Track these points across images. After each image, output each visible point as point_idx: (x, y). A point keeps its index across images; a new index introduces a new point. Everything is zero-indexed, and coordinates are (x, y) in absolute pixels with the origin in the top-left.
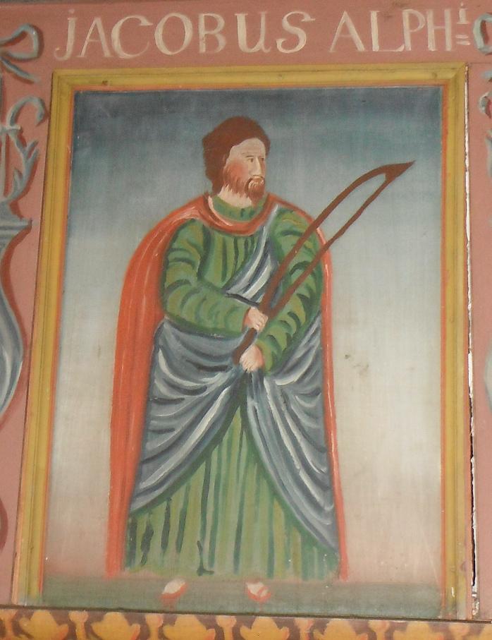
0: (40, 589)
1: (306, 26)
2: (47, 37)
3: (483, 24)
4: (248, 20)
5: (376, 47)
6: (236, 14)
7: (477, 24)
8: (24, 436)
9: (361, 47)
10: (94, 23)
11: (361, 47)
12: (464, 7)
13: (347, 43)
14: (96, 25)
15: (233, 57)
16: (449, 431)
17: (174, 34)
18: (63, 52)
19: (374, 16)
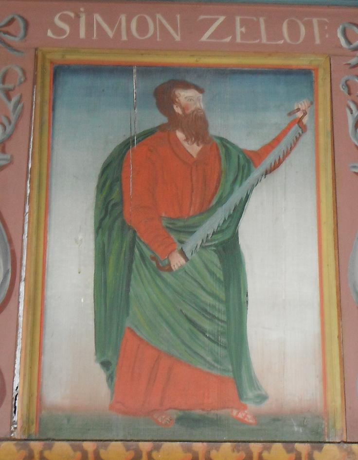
10: (157, 18)
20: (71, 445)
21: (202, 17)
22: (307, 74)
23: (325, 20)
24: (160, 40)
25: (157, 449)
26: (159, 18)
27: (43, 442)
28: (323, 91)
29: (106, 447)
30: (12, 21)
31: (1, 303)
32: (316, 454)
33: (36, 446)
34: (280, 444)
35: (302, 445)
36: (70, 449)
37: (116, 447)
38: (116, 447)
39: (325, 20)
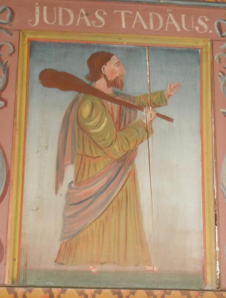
0: (107, 182)
1: (206, 22)
2: (16, 16)
3: (219, 25)
4: (48, 11)
5: (152, 27)
6: (59, 8)
7: (216, 24)
8: (149, 149)
9: (145, 27)
10: (81, 11)
11: (145, 27)
12: (38, 6)
13: (172, 26)
14: (170, 17)
15: (172, 31)
16: (22, 150)
17: (66, 17)
18: (34, 22)
19: (183, 16)
20: (112, 291)
21: (115, 11)
22: (193, 51)
23: (130, 12)
24: (135, 28)
25: (63, 292)
26: (137, 16)
27: (94, 289)
28: (206, 66)
29: (100, 293)
30: (4, 10)
31: (1, 196)
32: (97, 295)
33: (20, 291)
34: (5, 288)
35: (159, 291)
36: (76, 295)
37: (141, 293)
38: (141, 293)
39: (130, 12)
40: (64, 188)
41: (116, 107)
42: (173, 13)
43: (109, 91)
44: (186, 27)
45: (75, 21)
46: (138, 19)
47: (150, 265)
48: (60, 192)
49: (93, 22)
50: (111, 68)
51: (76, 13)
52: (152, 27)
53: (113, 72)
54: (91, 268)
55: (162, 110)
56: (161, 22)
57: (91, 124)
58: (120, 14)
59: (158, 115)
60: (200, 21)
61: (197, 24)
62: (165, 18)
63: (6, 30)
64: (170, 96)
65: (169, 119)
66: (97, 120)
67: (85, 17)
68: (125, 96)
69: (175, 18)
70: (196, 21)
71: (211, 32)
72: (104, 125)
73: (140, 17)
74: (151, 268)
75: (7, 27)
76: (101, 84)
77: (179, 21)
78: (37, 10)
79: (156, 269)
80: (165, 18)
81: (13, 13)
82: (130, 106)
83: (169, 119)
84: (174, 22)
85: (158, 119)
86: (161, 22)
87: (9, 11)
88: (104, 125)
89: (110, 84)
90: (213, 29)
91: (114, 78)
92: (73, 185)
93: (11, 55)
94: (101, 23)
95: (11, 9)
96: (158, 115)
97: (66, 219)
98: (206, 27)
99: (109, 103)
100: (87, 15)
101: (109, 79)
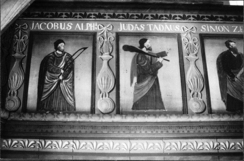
17: (131, 27)
18: (32, 28)
19: (82, 24)
21: (233, 27)
40: (133, 85)
41: (150, 57)
42: (167, 25)
43: (147, 52)
44: (42, 28)
45: (134, 29)
46: (155, 27)
47: (164, 109)
48: (132, 86)
49: (140, 29)
50: (147, 44)
51: (134, 26)
52: (160, 30)
53: (148, 46)
54: (144, 111)
55: (165, 58)
56: (163, 28)
57: (141, 63)
58: (149, 26)
59: (164, 59)
60: (176, 27)
61: (175, 28)
62: (164, 26)
63: (111, 32)
64: (168, 53)
65: (168, 61)
66: (143, 61)
67: (137, 27)
68: (153, 53)
69: (168, 26)
70: (175, 26)
71: (180, 30)
72: (146, 63)
73: (156, 26)
74: (165, 110)
75: (111, 31)
76: (144, 50)
77: (169, 27)
78: (33, 24)
79: (166, 110)
80: (164, 26)
81: (113, 27)
82: (155, 56)
83: (168, 61)
84: (168, 28)
85: (164, 61)
86: (163, 28)
87: (111, 26)
88: (146, 63)
89: (147, 49)
90: (181, 29)
91: (149, 47)
92: (136, 83)
93: (113, 41)
94: (204, 30)
95: (112, 25)
96: (164, 59)
97: (134, 95)
98: (178, 29)
99: (147, 56)
100: (138, 26)
101: (147, 47)
